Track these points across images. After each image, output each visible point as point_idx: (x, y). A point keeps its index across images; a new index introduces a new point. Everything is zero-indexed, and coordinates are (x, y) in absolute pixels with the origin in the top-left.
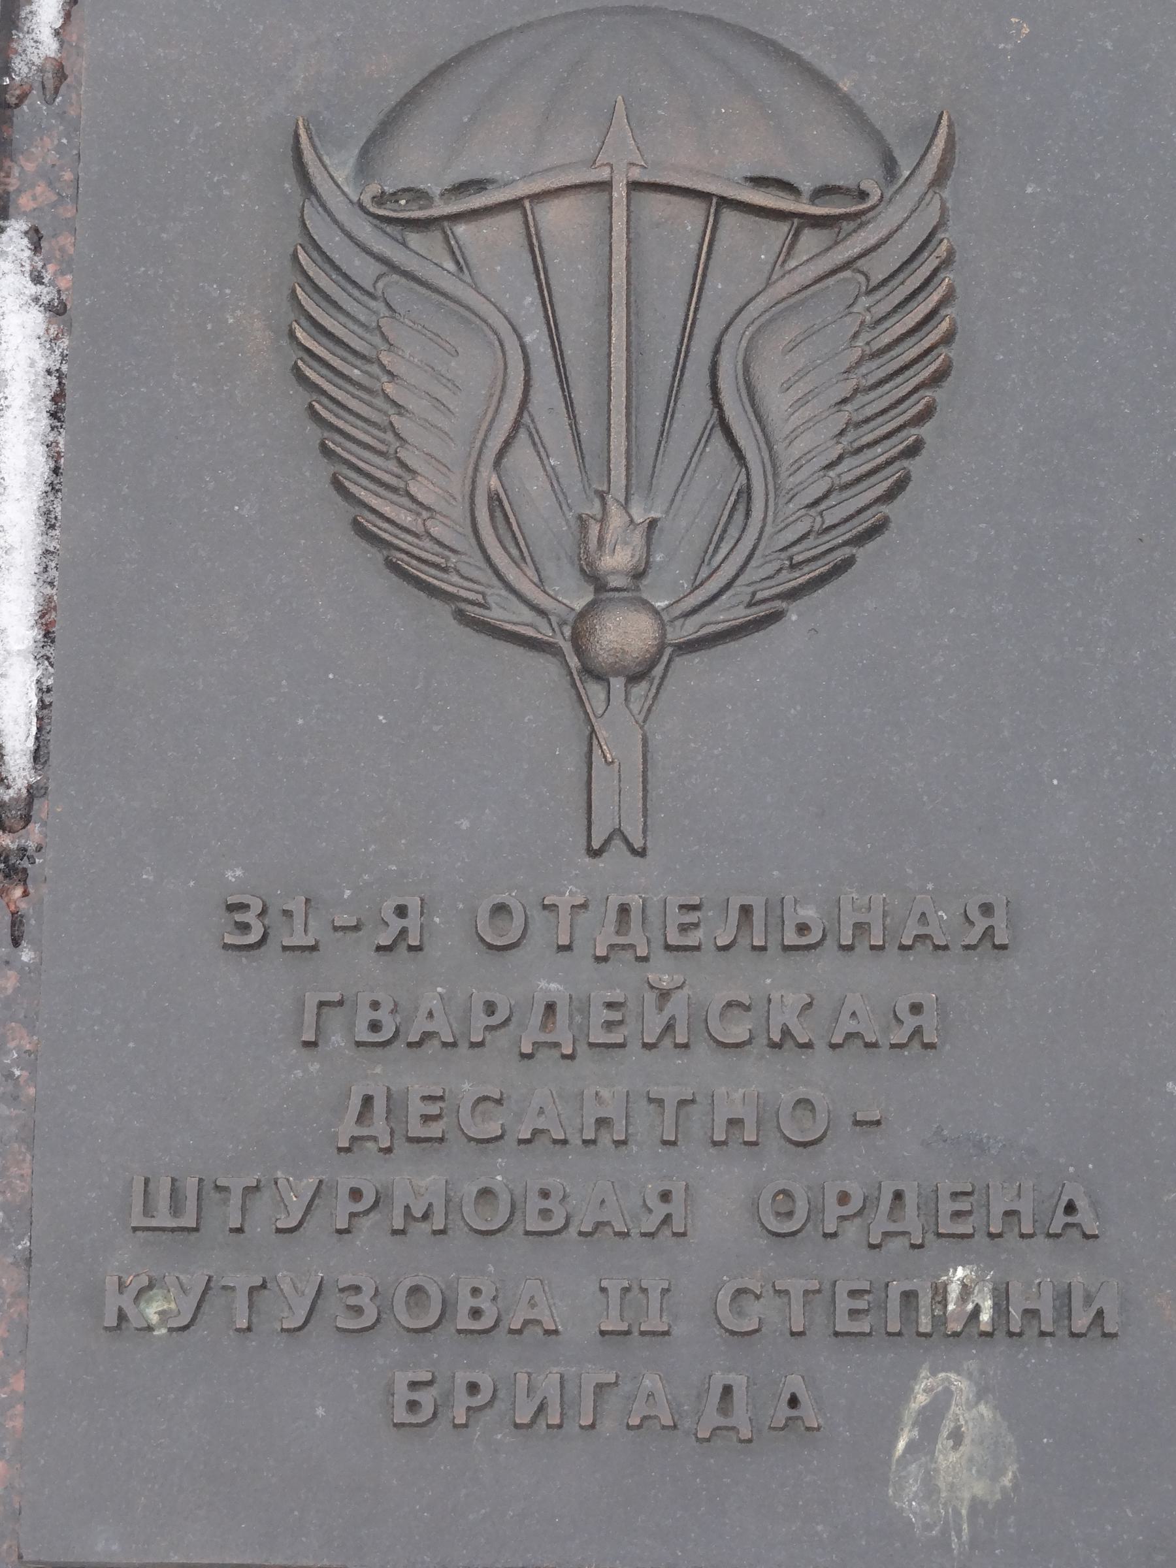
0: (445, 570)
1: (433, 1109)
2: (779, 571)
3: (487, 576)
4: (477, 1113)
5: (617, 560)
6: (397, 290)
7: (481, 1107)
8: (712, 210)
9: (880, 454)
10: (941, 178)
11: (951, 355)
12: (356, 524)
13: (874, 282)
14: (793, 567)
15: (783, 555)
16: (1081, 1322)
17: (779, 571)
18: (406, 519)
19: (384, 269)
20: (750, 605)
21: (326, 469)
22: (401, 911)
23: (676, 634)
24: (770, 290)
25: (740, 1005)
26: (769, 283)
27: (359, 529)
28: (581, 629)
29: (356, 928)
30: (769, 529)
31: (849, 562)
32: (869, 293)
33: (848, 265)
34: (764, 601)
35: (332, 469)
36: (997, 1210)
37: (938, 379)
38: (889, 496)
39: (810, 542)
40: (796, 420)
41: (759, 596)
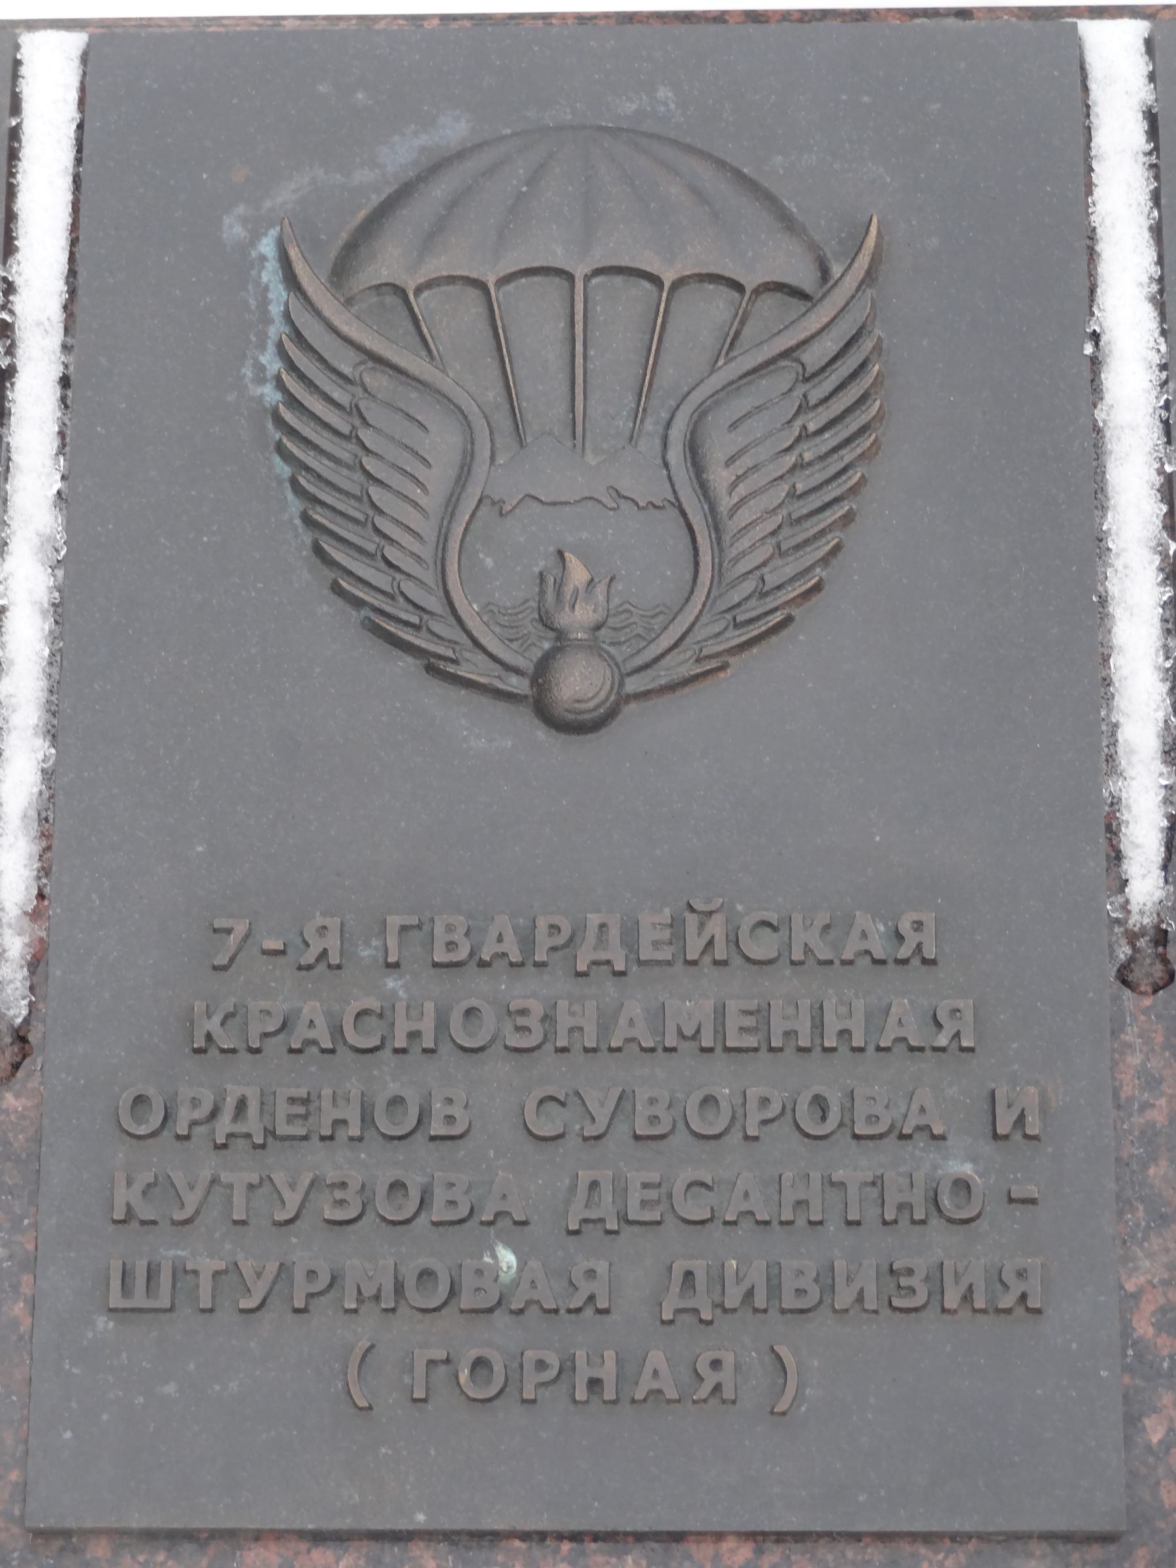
0: (417, 628)
1: (652, 1194)
2: (726, 629)
3: (457, 634)
4: (688, 1196)
5: (579, 617)
6: (378, 381)
7: (695, 1189)
8: (665, 295)
9: (830, 439)
10: (870, 277)
11: (854, 507)
12: (318, 550)
13: (810, 370)
14: (736, 626)
15: (729, 616)
16: (952, 1300)
17: (726, 629)
18: (381, 580)
19: (365, 357)
20: (698, 660)
21: (307, 538)
22: (716, 1364)
23: (633, 685)
24: (714, 377)
25: (703, 1184)
26: (713, 369)
27: (336, 589)
28: (542, 673)
29: (282, 953)
30: (714, 593)
31: (788, 621)
32: (807, 380)
33: (786, 354)
34: (710, 657)
35: (333, 575)
36: (789, 1197)
37: (848, 518)
38: (825, 561)
39: (753, 602)
40: (742, 490)
41: (705, 652)
